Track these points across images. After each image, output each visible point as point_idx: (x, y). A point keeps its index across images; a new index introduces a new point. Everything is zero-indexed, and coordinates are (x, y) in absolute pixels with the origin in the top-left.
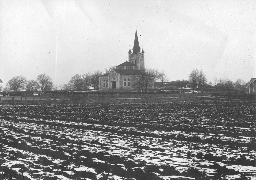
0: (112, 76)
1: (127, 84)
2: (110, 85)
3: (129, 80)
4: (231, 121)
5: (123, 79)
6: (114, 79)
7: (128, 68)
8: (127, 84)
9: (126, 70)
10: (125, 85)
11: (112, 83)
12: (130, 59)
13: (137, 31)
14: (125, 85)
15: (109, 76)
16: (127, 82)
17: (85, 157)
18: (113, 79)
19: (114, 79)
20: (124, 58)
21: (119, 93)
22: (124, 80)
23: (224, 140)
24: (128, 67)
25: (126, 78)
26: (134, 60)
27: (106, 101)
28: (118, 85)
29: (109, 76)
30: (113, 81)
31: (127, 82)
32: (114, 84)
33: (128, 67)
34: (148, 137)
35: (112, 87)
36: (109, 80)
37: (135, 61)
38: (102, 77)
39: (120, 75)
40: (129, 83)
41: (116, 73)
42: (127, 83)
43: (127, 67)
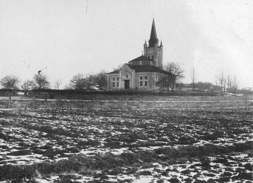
1: (144, 84)
2: (121, 85)
6: (127, 76)
7: (146, 64)
9: (141, 66)
11: (124, 82)
15: (120, 74)
18: (125, 77)
19: (127, 76)
20: (139, 52)
22: (139, 78)
26: (151, 54)
28: (132, 85)
29: (120, 74)
30: (126, 79)
31: (144, 80)
35: (123, 87)
36: (121, 78)
38: (112, 75)
41: (130, 70)
43: (143, 63)
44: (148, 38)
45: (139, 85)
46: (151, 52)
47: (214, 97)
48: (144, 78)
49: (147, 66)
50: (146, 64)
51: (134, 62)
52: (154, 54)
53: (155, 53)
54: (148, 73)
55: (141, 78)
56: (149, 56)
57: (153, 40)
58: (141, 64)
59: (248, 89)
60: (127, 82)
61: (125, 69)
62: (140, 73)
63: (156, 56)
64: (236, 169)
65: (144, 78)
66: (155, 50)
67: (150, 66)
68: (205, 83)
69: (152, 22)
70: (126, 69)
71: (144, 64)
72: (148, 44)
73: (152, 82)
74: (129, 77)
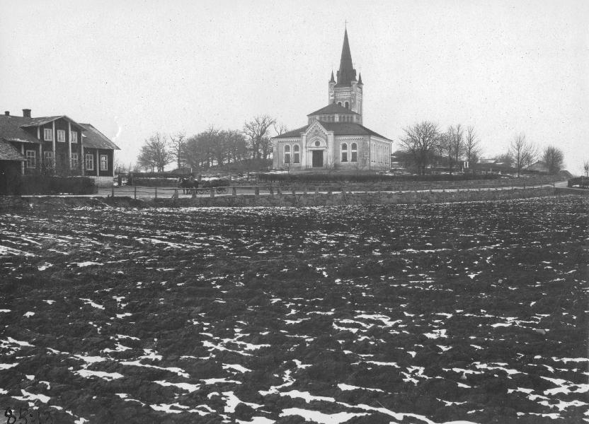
0: (313, 136)
1: (350, 158)
2: (306, 160)
3: (354, 146)
4: (439, 318)
5: (339, 146)
6: (318, 144)
7: (346, 120)
8: (350, 158)
9: (337, 123)
10: (345, 159)
11: (311, 154)
12: (333, 98)
13: (348, 34)
14: (345, 159)
15: (304, 137)
16: (349, 151)
17: (469, 412)
18: (314, 145)
19: (318, 144)
20: (323, 99)
21: (479, 177)
22: (341, 147)
23: (344, 329)
24: (344, 117)
25: (298, 144)
26: (343, 99)
27: (415, 196)
28: (328, 158)
29: (304, 137)
30: (316, 149)
31: (349, 151)
32: (318, 156)
33: (344, 117)
34: (482, 363)
35: (311, 163)
36: (306, 147)
37: (347, 103)
38: (282, 140)
39: (335, 135)
40: (354, 155)
41: (324, 130)
42: (351, 155)
43: (340, 118)
44: (336, 67)
45: (341, 159)
46: (344, 95)
47: (493, 182)
48: (349, 146)
49: (347, 123)
50: (346, 120)
51: (323, 116)
52: (350, 99)
53: (353, 98)
54: (359, 137)
55: (345, 147)
56: (340, 103)
57: (347, 76)
58: (337, 119)
59: (493, 162)
60: (318, 156)
61: (314, 131)
62: (343, 138)
63: (355, 102)
64: (282, 412)
65: (349, 146)
66: (353, 93)
67: (352, 123)
68: (223, 134)
69: (343, 40)
70: (316, 131)
71: (331, 119)
72: (336, 79)
73: (367, 154)
74: (323, 144)
